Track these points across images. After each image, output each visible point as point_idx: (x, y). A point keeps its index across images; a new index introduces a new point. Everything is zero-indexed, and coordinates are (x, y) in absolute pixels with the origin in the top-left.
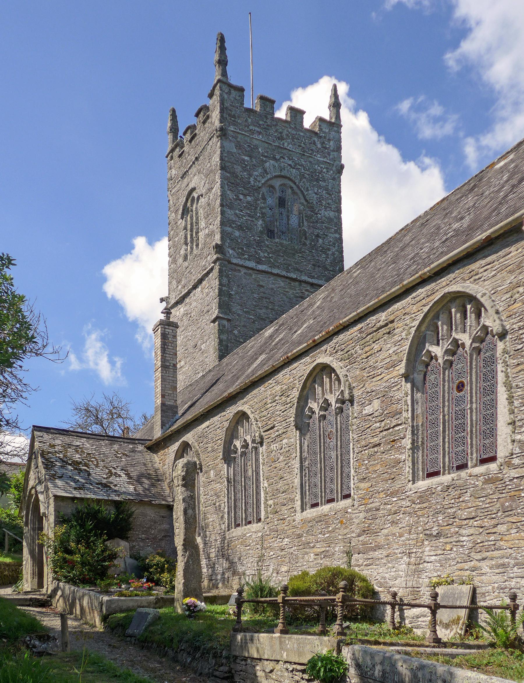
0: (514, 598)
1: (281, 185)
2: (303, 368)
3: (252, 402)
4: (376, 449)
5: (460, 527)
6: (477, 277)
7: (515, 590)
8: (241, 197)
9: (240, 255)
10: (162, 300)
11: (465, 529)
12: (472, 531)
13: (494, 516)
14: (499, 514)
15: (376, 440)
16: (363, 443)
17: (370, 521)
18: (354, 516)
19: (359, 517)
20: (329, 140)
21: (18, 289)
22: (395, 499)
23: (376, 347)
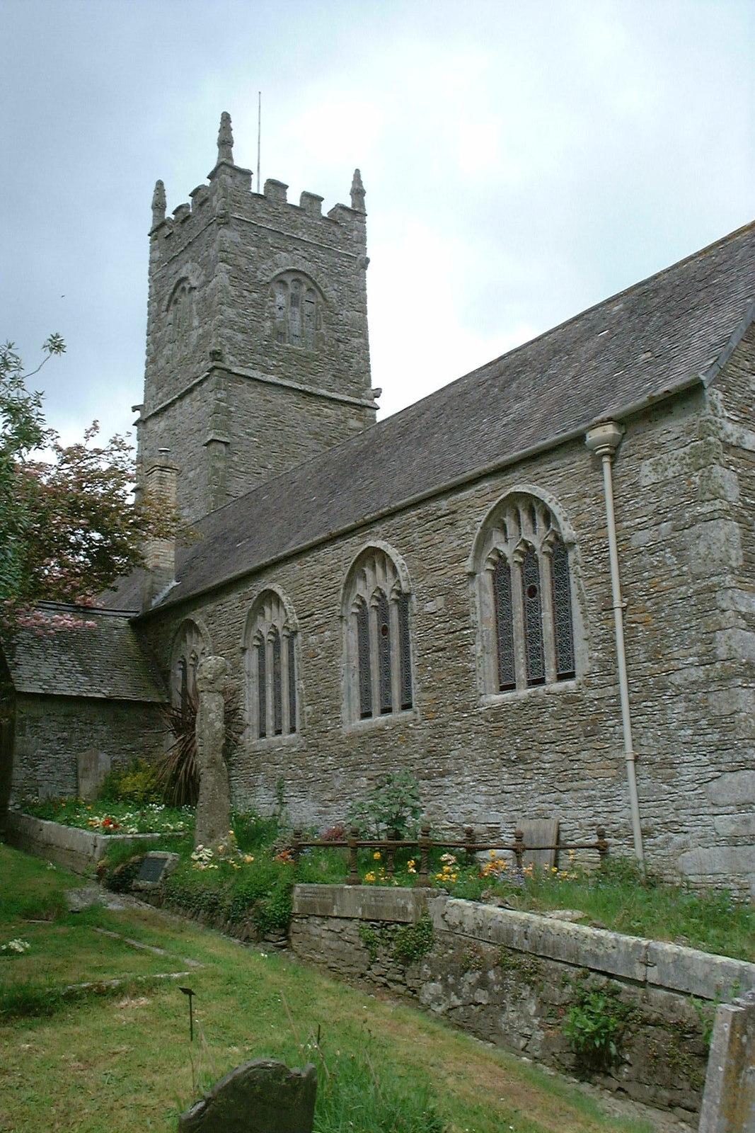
0: (601, 835)
1: (293, 281)
2: (352, 548)
3: (283, 581)
4: (440, 654)
5: (540, 752)
6: (543, 480)
7: (603, 827)
8: (245, 293)
9: (243, 364)
10: (135, 409)
11: (546, 754)
12: (552, 757)
13: (576, 741)
14: (582, 739)
15: (440, 643)
16: (425, 645)
17: (436, 741)
18: (417, 732)
19: (422, 733)
20: (352, 230)
21: (39, 461)
22: (466, 715)
23: (437, 538)
